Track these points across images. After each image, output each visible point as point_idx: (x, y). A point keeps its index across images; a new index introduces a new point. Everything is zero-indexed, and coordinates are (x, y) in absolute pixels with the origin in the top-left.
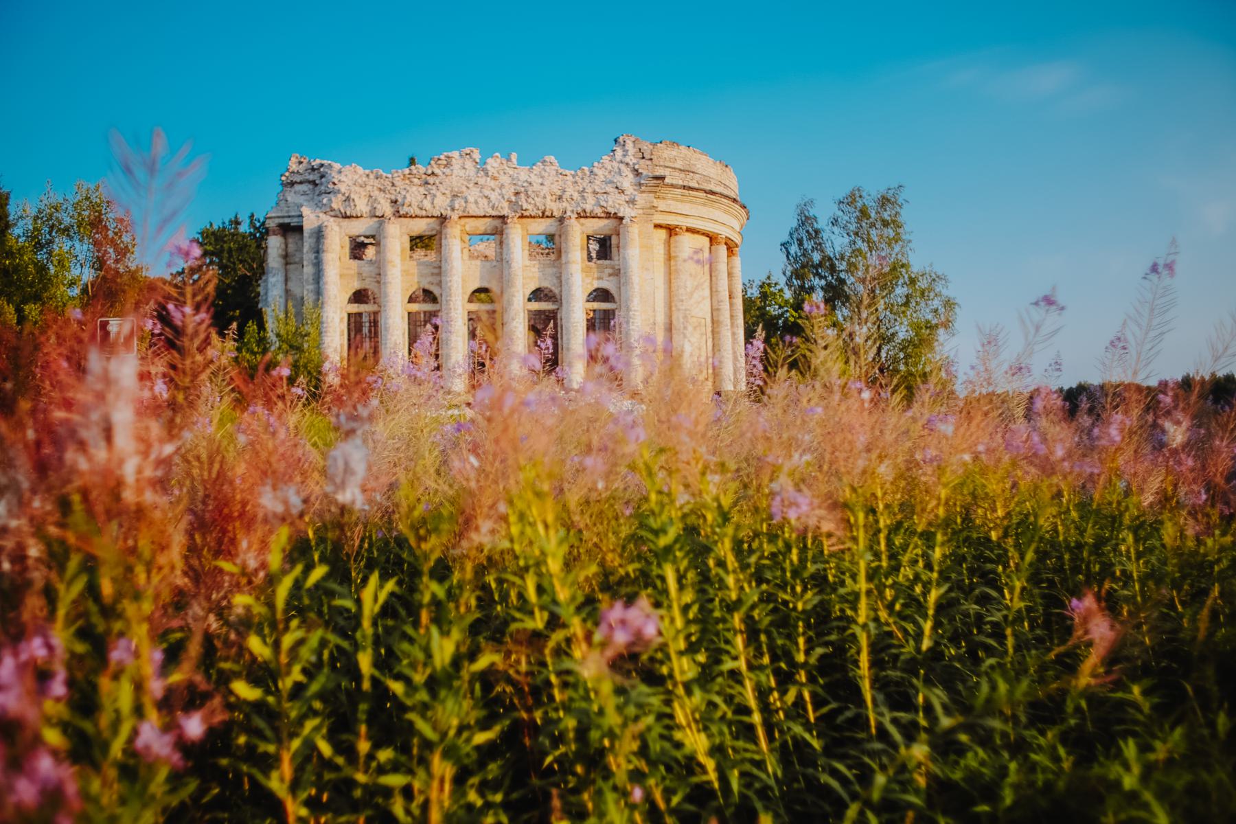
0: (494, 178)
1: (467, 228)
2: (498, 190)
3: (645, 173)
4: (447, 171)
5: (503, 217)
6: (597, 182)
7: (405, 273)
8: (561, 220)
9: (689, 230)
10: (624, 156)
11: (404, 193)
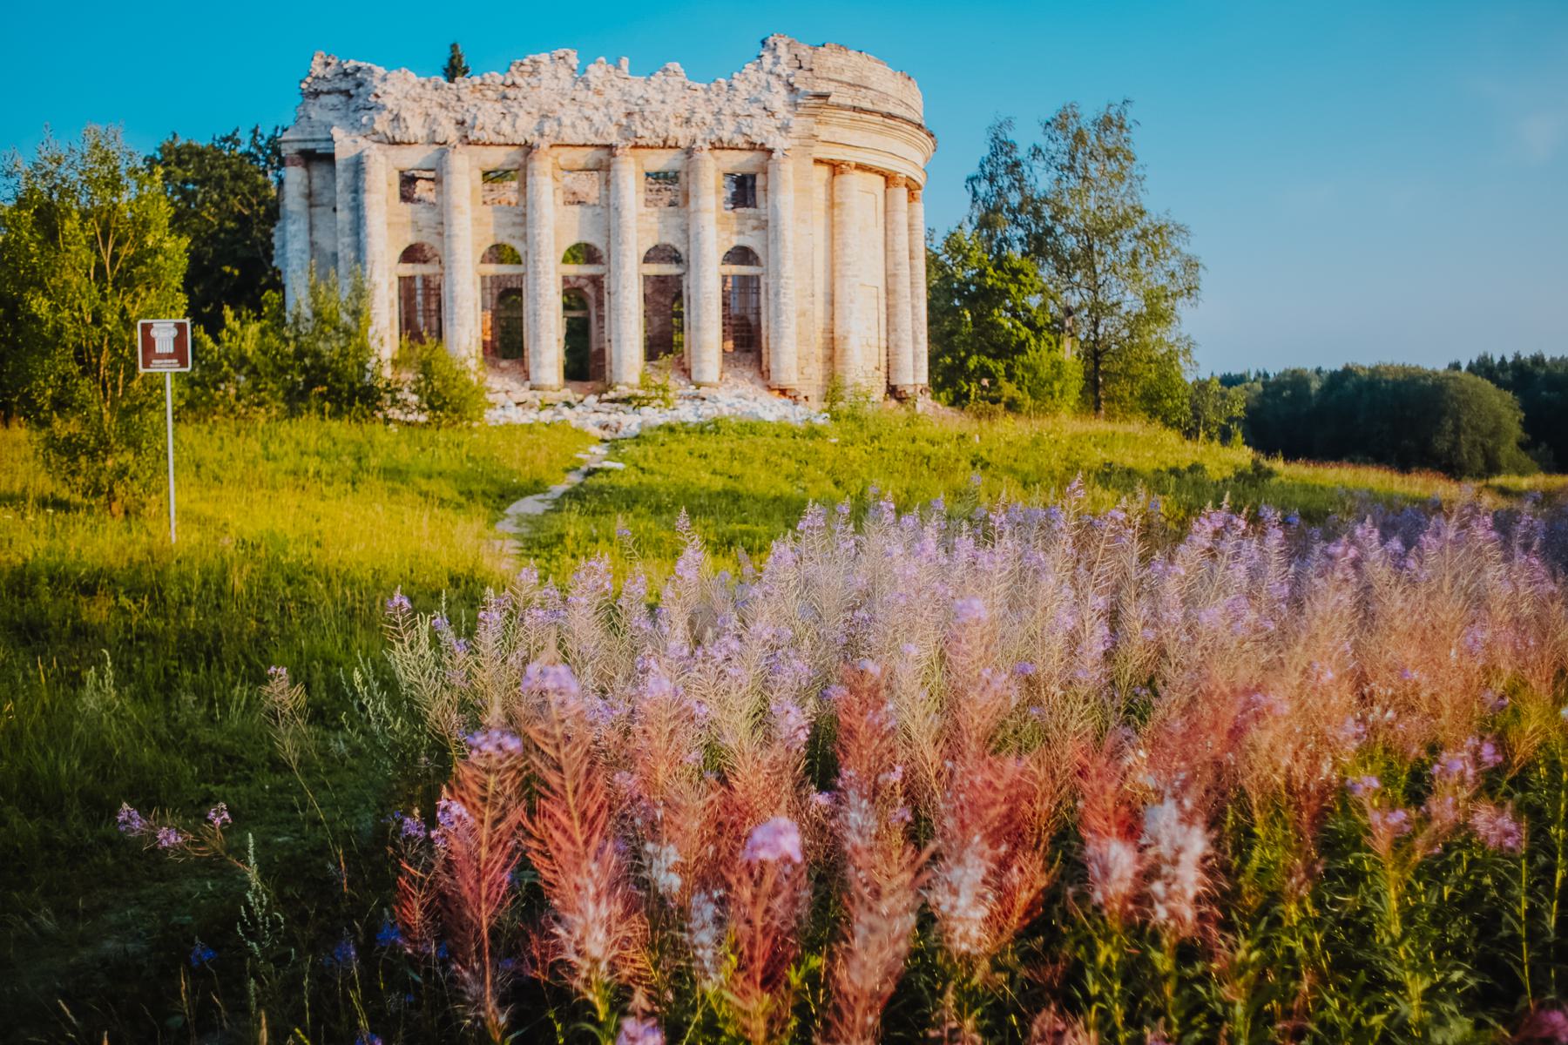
0: (598, 93)
1: (561, 161)
2: (603, 109)
3: (803, 88)
4: (533, 81)
5: (610, 147)
6: (738, 100)
7: (477, 221)
8: (689, 152)
9: (860, 167)
10: (775, 64)
11: (473, 110)
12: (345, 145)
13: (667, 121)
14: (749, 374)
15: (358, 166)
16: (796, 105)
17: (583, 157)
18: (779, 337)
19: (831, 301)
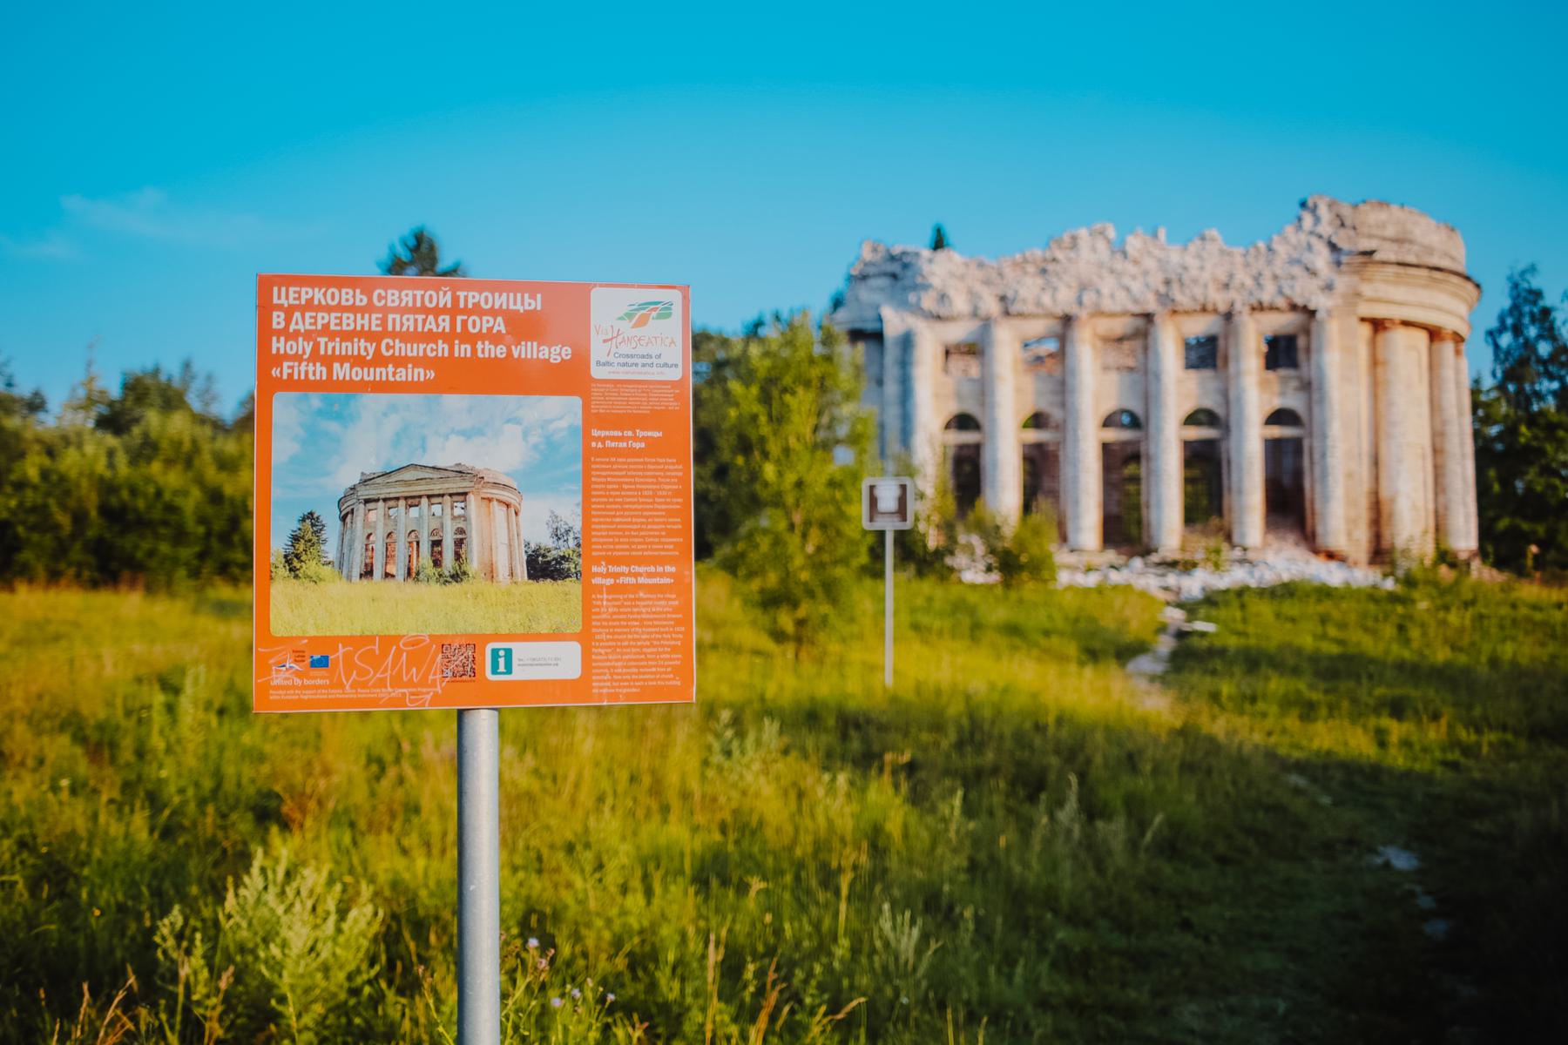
0: (1136, 262)
4: (1072, 255)
7: (1018, 390)
9: (1406, 323)
12: (894, 322)
13: (1206, 286)
14: (1291, 538)
15: (907, 342)
16: (1339, 264)
17: (1120, 326)
18: (1326, 499)
19: (1376, 462)
